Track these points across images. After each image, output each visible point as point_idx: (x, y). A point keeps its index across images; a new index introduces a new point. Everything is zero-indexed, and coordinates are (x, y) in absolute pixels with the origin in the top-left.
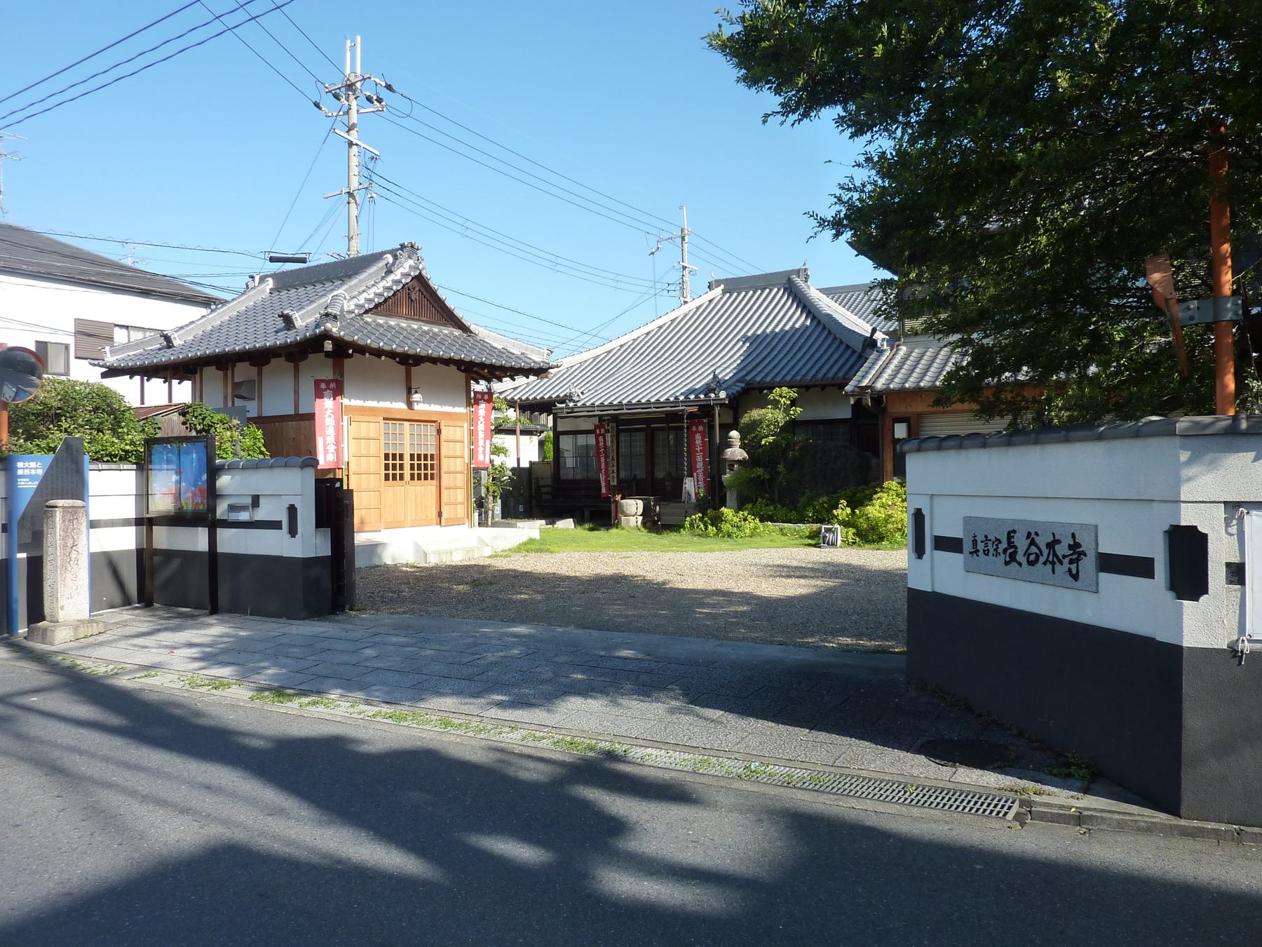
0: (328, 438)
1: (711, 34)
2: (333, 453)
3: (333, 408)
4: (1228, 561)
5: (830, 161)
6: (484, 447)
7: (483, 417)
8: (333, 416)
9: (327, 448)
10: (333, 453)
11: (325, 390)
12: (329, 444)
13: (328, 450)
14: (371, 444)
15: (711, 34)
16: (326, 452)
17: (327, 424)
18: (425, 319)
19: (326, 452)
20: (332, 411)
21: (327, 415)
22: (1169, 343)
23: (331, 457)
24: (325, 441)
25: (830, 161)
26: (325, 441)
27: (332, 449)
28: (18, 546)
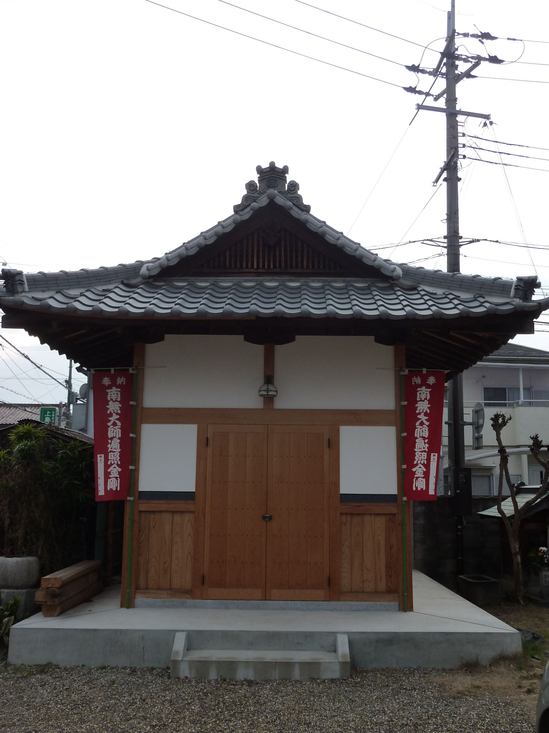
0: (111, 456)
1: (300, 680)
2: (116, 478)
3: (119, 412)
4: (50, 349)
5: (469, 414)
6: (427, 466)
7: (426, 414)
8: (119, 423)
9: (109, 471)
10: (116, 478)
11: (110, 387)
12: (111, 464)
13: (110, 473)
14: (465, 401)
15: (300, 680)
16: (107, 475)
17: (110, 435)
18: (299, 270)
19: (107, 475)
20: (118, 417)
21: (111, 423)
22: (33, 446)
23: (114, 484)
24: (106, 459)
25: (469, 414)
26: (106, 459)
27: (115, 471)
28: (523, 389)
